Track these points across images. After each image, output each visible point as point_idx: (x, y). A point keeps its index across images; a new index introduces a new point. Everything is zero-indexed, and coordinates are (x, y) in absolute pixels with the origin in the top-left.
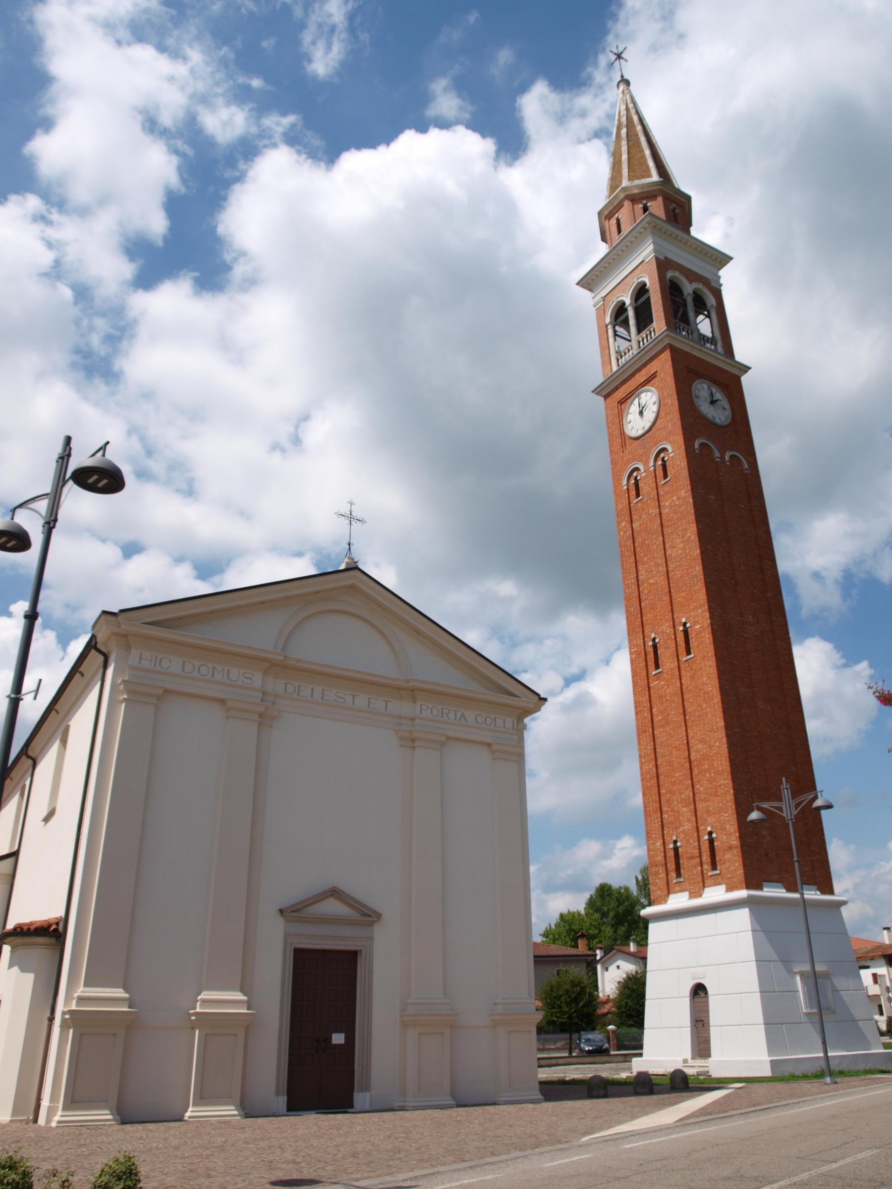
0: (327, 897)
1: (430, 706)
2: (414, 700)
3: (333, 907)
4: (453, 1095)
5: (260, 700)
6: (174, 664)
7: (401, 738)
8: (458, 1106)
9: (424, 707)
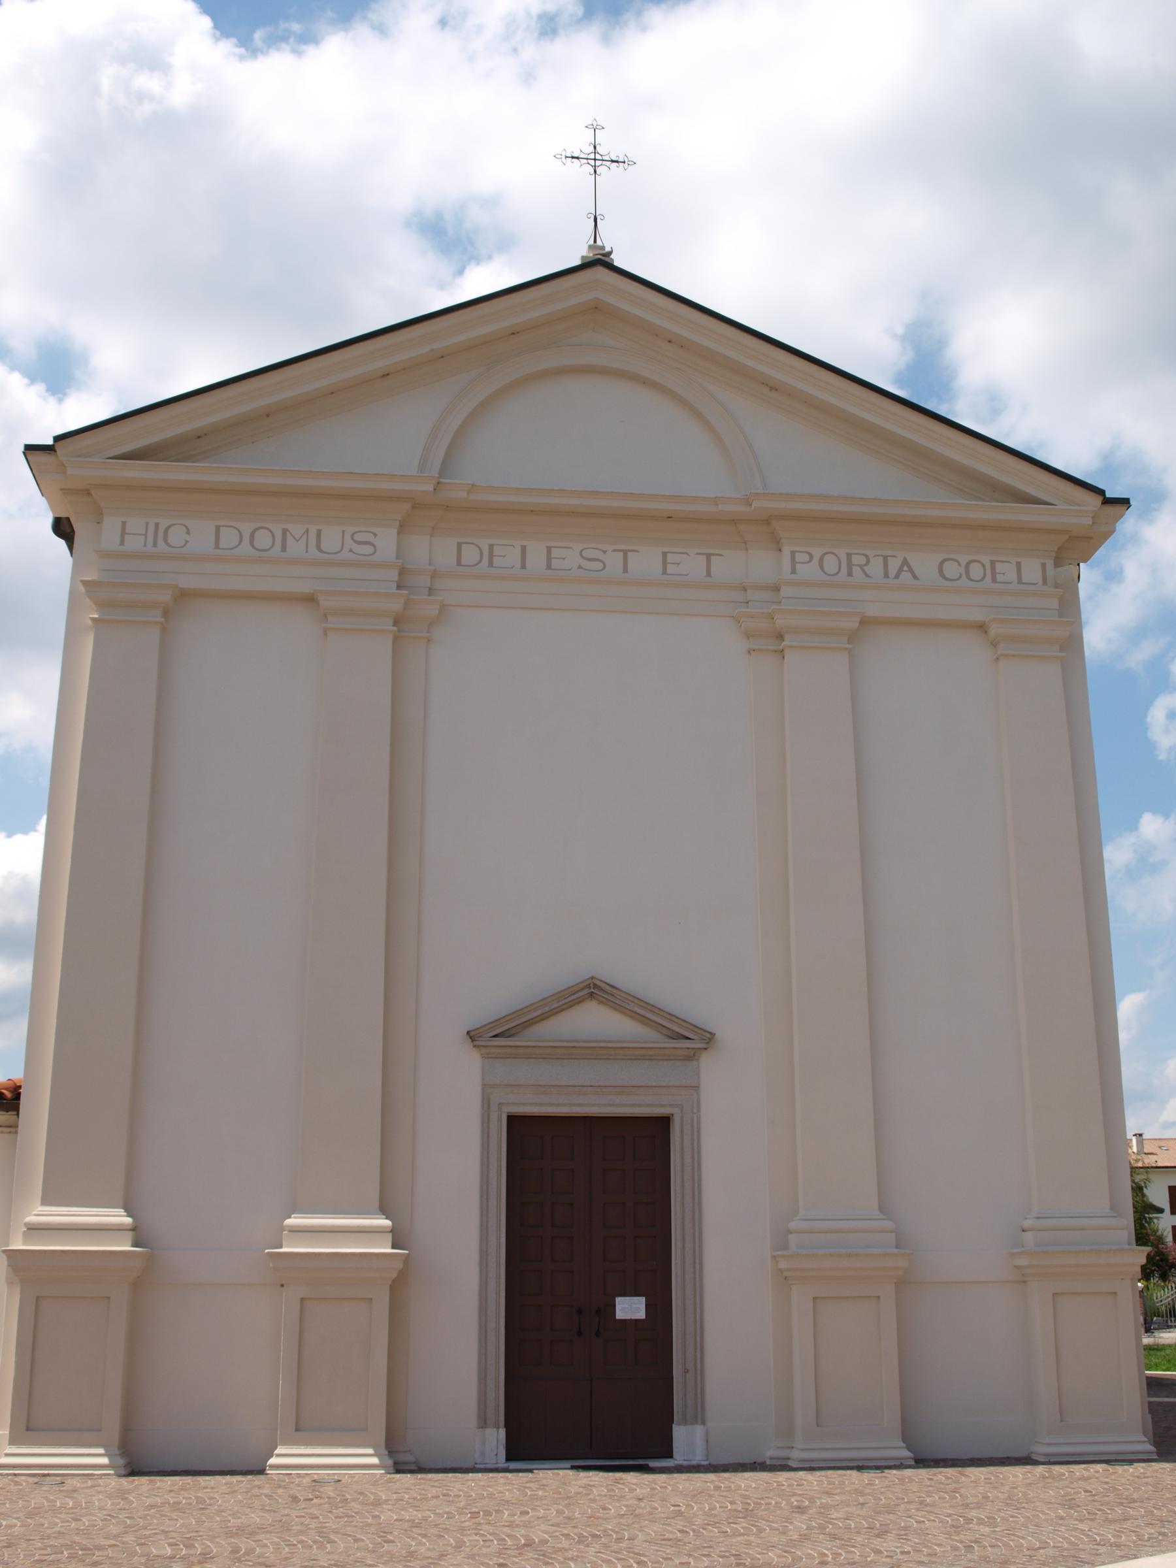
0: (579, 1001)
1: (817, 552)
2: (777, 544)
3: (594, 1022)
4: (908, 1439)
5: (395, 585)
6: (197, 535)
7: (749, 635)
8: (922, 1462)
9: (800, 557)
